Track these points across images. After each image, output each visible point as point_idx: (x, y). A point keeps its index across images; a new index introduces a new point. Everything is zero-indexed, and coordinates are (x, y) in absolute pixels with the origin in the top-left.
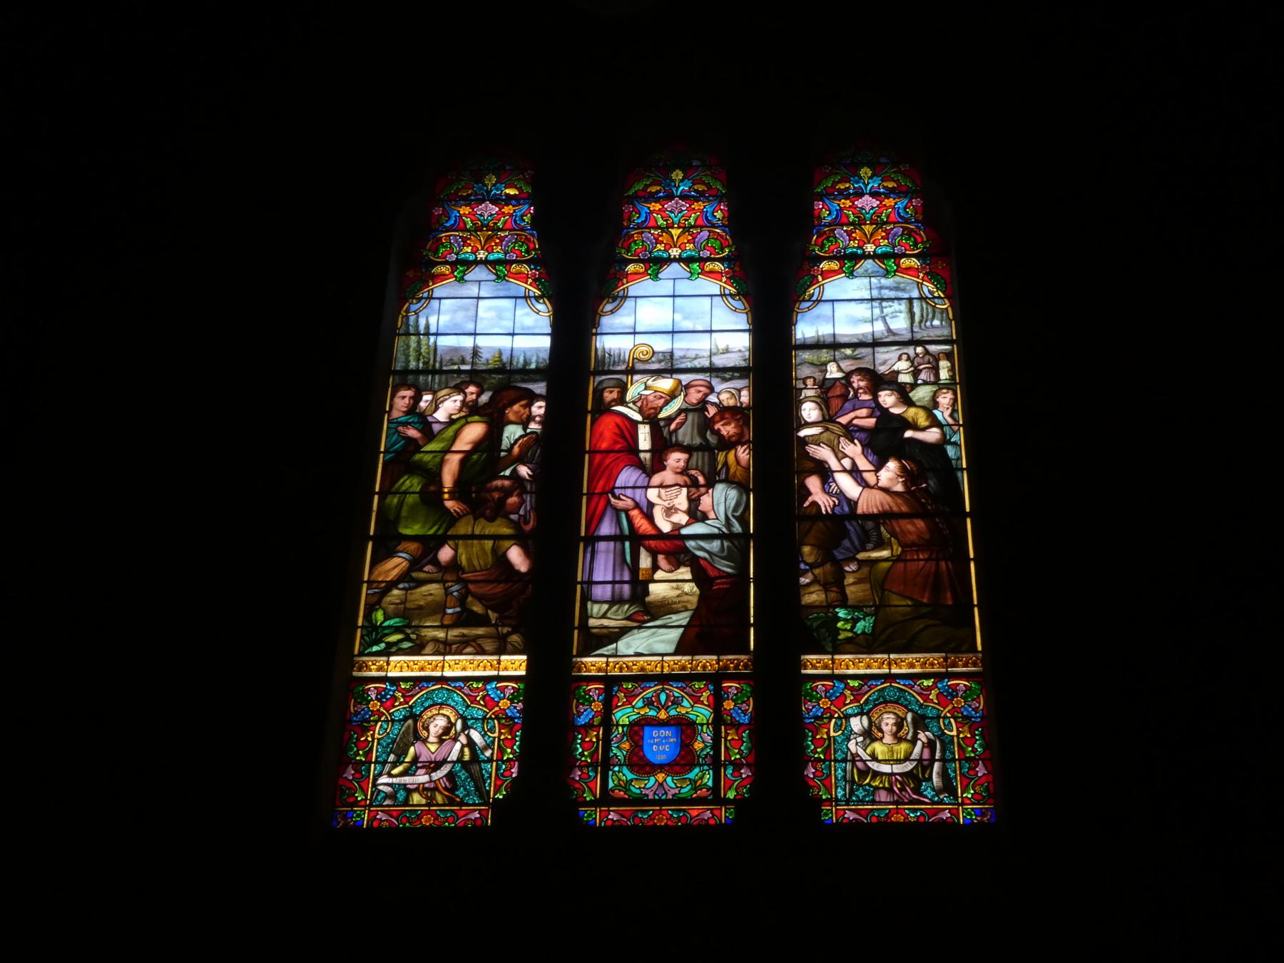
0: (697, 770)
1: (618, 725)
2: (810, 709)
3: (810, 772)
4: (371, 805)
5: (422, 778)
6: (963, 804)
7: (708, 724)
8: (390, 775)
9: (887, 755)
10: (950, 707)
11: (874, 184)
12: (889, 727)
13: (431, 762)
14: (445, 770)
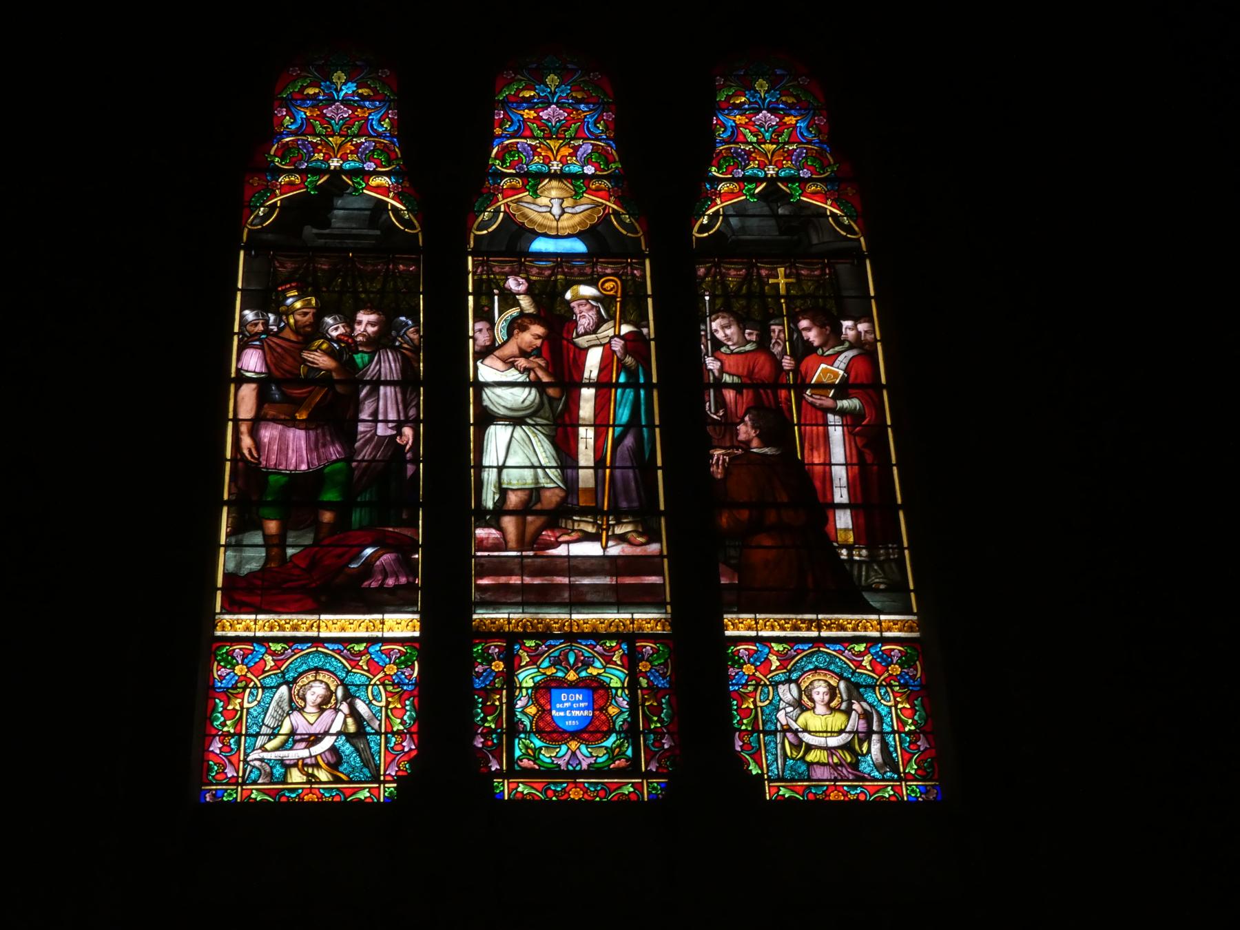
1: (521, 688)
3: (216, 746)
4: (244, 783)
5: (300, 752)
6: (385, 782)
7: (623, 688)
8: (263, 748)
9: (822, 726)
10: (381, 675)
11: (348, 89)
12: (821, 696)
13: (311, 735)
14: (327, 742)
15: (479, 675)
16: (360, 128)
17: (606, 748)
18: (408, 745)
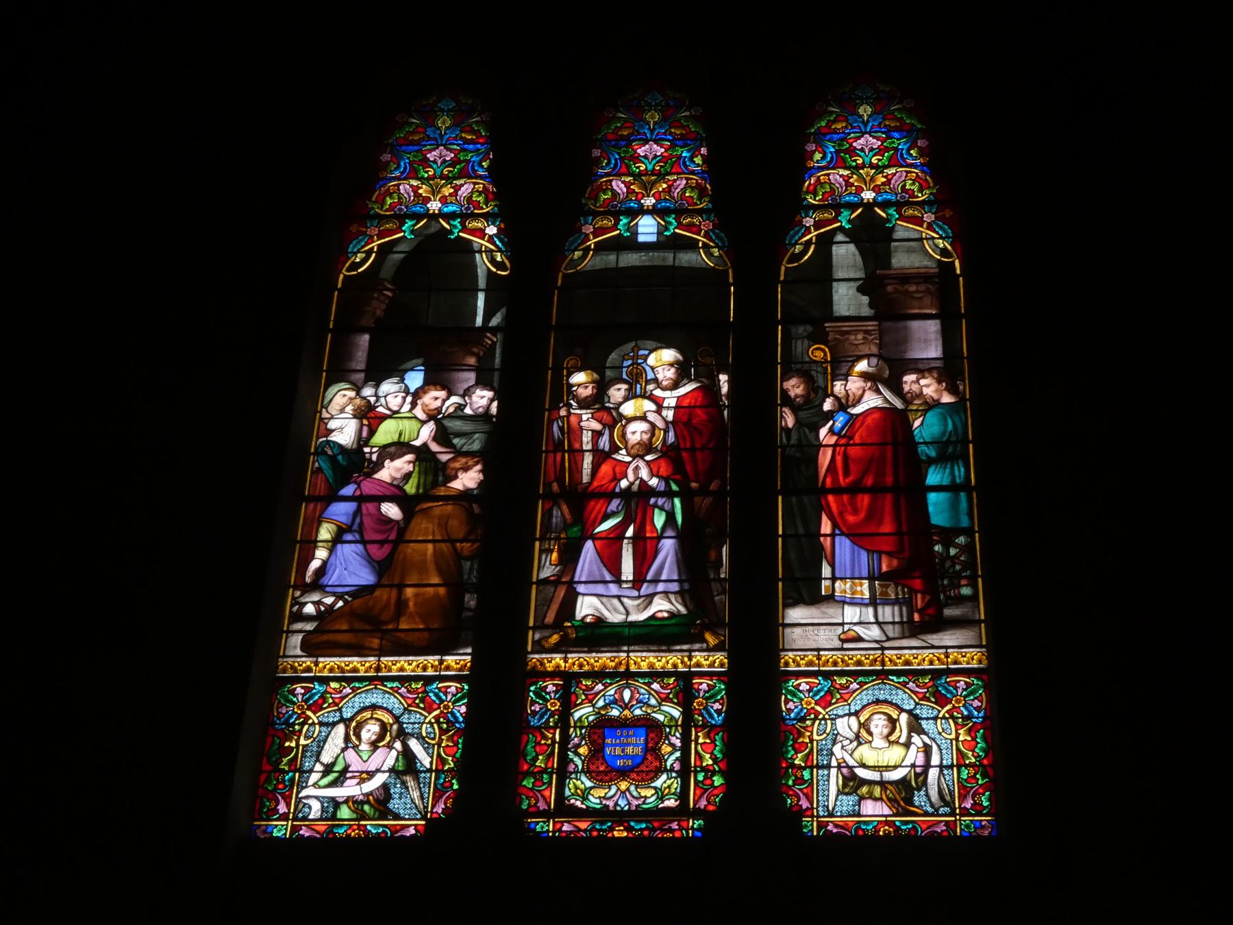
0: (664, 777)
2: (790, 707)
8: (315, 785)
10: (949, 707)
15: (534, 713)
16: (890, 159)
17: (655, 788)
18: (718, 781)
